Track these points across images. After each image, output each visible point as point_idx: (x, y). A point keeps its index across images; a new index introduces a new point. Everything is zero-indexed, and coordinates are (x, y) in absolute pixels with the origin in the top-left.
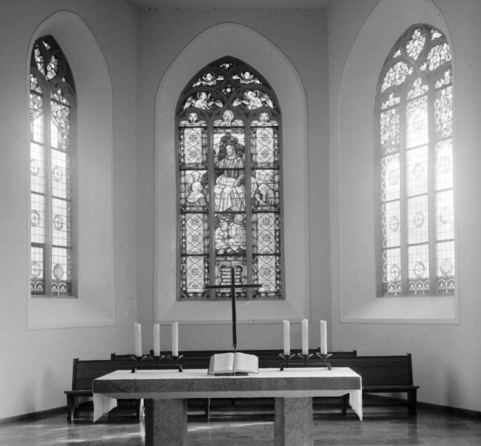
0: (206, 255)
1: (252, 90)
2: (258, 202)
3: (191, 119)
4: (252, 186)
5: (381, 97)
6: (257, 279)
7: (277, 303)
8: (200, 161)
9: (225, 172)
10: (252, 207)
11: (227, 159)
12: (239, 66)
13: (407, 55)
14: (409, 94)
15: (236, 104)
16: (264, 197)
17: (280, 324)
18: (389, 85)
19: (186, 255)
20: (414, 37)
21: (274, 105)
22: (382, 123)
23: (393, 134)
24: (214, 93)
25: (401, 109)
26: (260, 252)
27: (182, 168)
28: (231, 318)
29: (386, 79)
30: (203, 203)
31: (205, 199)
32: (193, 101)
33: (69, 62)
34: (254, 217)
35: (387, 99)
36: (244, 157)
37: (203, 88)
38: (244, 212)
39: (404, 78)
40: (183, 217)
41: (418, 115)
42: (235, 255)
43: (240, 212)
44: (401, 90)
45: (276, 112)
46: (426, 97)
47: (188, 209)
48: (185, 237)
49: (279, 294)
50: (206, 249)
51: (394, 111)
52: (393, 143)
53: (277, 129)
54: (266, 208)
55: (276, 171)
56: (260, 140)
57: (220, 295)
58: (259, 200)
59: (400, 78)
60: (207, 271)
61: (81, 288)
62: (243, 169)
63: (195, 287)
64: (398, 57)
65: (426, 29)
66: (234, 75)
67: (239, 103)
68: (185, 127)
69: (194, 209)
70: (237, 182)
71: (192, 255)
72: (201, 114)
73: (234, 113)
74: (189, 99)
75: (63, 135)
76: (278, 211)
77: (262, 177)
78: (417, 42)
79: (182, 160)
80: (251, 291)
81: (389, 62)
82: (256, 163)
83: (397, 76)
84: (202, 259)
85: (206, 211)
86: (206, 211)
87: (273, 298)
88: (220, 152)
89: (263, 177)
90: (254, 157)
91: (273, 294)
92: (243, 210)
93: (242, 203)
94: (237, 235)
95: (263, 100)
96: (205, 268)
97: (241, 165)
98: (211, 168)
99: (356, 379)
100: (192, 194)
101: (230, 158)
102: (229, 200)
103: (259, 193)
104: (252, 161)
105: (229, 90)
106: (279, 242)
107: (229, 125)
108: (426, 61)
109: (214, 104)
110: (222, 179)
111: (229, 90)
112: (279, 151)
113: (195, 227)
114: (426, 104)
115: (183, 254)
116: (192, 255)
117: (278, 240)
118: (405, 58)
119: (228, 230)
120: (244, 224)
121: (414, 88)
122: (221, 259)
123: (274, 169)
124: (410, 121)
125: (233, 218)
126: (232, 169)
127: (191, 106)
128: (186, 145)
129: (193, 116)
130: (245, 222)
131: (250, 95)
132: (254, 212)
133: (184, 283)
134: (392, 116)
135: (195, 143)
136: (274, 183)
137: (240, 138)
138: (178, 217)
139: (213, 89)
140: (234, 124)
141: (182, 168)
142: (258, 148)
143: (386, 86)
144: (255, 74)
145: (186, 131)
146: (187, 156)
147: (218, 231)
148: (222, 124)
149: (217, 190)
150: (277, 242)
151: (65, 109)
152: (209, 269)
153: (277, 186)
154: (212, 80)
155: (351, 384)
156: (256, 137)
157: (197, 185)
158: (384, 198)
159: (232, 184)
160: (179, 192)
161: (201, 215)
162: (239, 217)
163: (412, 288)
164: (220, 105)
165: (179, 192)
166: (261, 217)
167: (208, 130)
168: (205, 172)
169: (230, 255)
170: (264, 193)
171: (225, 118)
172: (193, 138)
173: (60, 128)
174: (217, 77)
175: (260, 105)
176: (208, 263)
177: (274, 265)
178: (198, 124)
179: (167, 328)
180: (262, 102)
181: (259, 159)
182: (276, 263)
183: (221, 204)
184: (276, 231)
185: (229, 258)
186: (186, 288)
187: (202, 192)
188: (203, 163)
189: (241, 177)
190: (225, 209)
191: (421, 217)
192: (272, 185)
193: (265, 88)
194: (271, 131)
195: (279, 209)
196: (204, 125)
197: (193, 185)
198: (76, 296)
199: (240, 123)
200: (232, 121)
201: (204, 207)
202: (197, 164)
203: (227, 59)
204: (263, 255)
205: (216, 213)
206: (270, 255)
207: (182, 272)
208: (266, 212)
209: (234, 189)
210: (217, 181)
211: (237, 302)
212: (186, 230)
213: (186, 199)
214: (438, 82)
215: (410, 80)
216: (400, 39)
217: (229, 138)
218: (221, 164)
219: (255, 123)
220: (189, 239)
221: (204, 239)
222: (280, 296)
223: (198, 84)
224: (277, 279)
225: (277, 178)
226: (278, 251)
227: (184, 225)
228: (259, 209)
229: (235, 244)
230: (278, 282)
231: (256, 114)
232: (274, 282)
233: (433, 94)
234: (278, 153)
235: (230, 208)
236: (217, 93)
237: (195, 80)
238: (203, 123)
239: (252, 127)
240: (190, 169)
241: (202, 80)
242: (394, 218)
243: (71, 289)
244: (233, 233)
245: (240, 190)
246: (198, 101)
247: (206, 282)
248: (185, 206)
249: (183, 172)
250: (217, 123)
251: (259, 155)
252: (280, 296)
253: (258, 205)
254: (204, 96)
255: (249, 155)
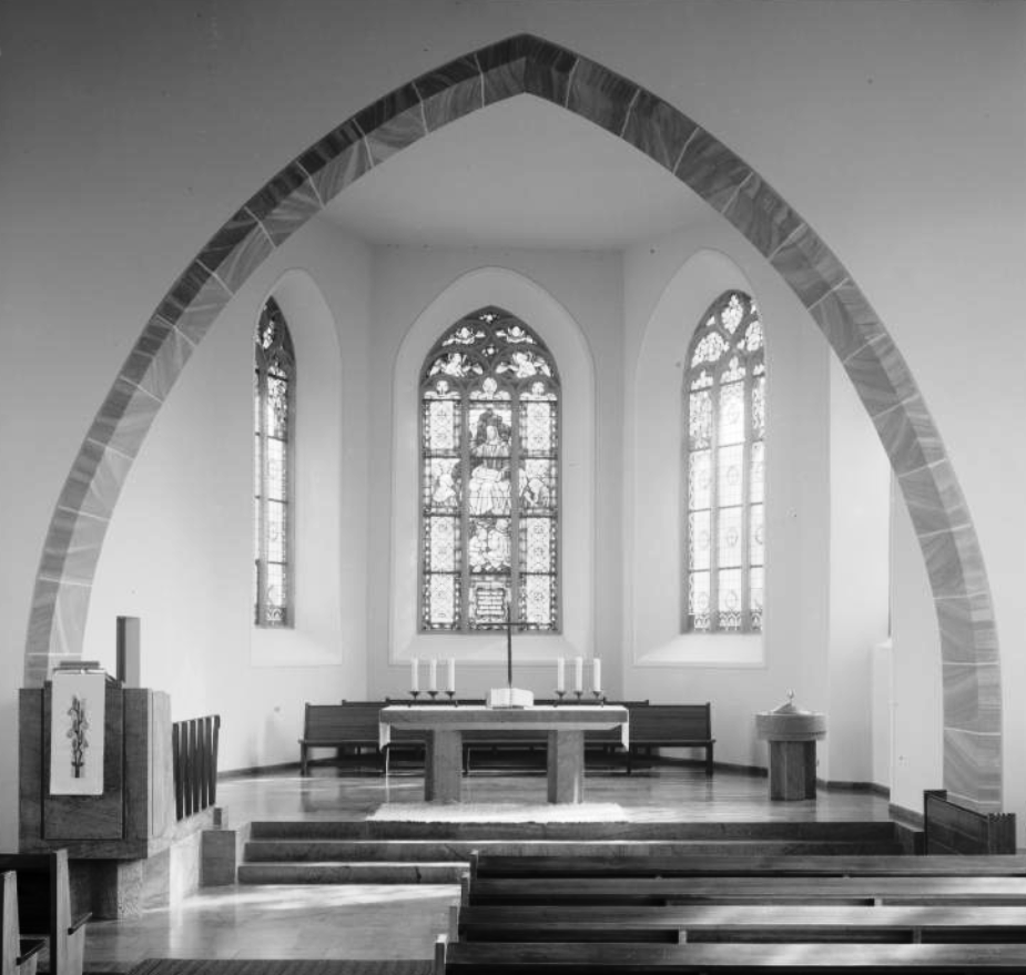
0: (458, 574)
1: (522, 351)
2: (529, 503)
3: (439, 389)
4: (521, 481)
5: (691, 374)
6: (525, 607)
7: (552, 639)
8: (451, 447)
9: (485, 462)
10: (520, 509)
11: (488, 444)
12: (505, 319)
13: (722, 325)
14: (724, 376)
15: (501, 369)
16: (536, 497)
17: (555, 666)
18: (700, 360)
19: (430, 573)
20: (730, 304)
21: (551, 372)
22: (692, 408)
23: (705, 425)
24: (472, 355)
25: (715, 391)
26: (529, 569)
27: (426, 455)
28: (507, 659)
29: (697, 351)
30: (454, 503)
31: (457, 497)
32: (443, 365)
33: (289, 325)
34: (523, 523)
35: (698, 377)
36: (510, 442)
37: (456, 348)
38: (509, 517)
39: (718, 354)
40: (427, 521)
41: (733, 402)
42: (495, 573)
43: (503, 517)
44: (715, 369)
45: (554, 384)
46: (742, 383)
47: (433, 510)
48: (428, 549)
49: (555, 628)
50: (457, 565)
51: (705, 394)
52: (704, 435)
53: (555, 405)
54: (539, 511)
55: (553, 462)
56: (533, 419)
57: (475, 627)
58: (529, 499)
59: (714, 353)
60: (457, 594)
61: (301, 611)
62: (509, 458)
63: (442, 615)
64: (711, 326)
65: (745, 299)
66: (499, 329)
67: (505, 369)
68: (431, 400)
69: (442, 510)
70: (500, 474)
71: (438, 573)
72: (454, 383)
73: (497, 382)
74: (438, 362)
75: (279, 418)
76: (555, 515)
77: (535, 470)
78: (734, 311)
79: (427, 445)
80: (513, 625)
81: (701, 331)
82: (526, 451)
83: (711, 350)
84: (451, 578)
85: (459, 513)
86: (459, 513)
87: (546, 632)
88: (479, 434)
89: (534, 473)
90: (524, 442)
91: (546, 627)
92: (508, 513)
93: (507, 503)
94: (499, 546)
95: (537, 365)
96: (456, 590)
97: (506, 453)
98: (466, 457)
99: (623, 713)
100: (440, 490)
101: (492, 443)
102: (490, 499)
103: (530, 491)
104: (521, 447)
105: (491, 351)
106: (555, 558)
107: (491, 398)
108: (744, 337)
109: (471, 371)
110: (480, 472)
111: (491, 351)
112: (557, 435)
113: (443, 535)
114: (742, 393)
115: (425, 571)
116: (438, 573)
117: (554, 554)
118: (719, 328)
119: (487, 540)
120: (509, 532)
121: (730, 370)
122: (476, 578)
123: (550, 459)
124: (725, 411)
125: (494, 524)
126: (493, 458)
127: (440, 372)
128: (432, 424)
129: (443, 385)
130: (510, 529)
131: (519, 358)
132: (522, 516)
133: (427, 610)
134: (703, 401)
135: (445, 421)
136: (550, 477)
137: (506, 416)
138: (420, 522)
139: (470, 350)
140: (498, 397)
141: (426, 455)
142: (529, 430)
143: (697, 360)
144: (528, 331)
145: (433, 405)
146: (433, 439)
147: (473, 541)
148: (482, 397)
149: (473, 485)
150: (552, 558)
151: (281, 385)
152: (461, 592)
153: (553, 481)
154: (469, 337)
155: (620, 717)
156: (526, 416)
157: (447, 480)
158: (692, 504)
159: (492, 478)
160: (422, 487)
161: (451, 519)
162: (502, 523)
163: (723, 623)
164: (479, 371)
165: (422, 487)
166: (531, 524)
167: (463, 405)
168: (457, 461)
169: (489, 574)
170: (536, 491)
171: (485, 389)
172: (442, 415)
173: (277, 409)
174: (475, 333)
175: (532, 372)
176: (460, 584)
177: (548, 588)
178: (448, 396)
179: (442, 668)
180: (536, 368)
181: (531, 445)
182: (551, 585)
183: (477, 506)
184: (551, 542)
185: (488, 578)
186: (430, 617)
187: (453, 487)
188: (455, 449)
189: (506, 468)
190: (483, 512)
191: (735, 535)
192: (547, 480)
193: (539, 350)
194: (547, 407)
195: (556, 513)
196: (457, 398)
197: (441, 478)
198: (292, 626)
199: (505, 395)
200: (495, 393)
201: (455, 508)
202: (447, 451)
203: (490, 310)
204: (534, 574)
205: (472, 516)
206: (542, 574)
207: (424, 595)
208: (538, 516)
209: (496, 485)
210: (473, 474)
211: (513, 638)
212: (430, 539)
213: (431, 497)
214: (756, 368)
215: (726, 357)
216: (713, 305)
217: (491, 416)
218: (480, 451)
219: (525, 396)
220: (434, 551)
221: (455, 551)
222: (555, 630)
223: (450, 341)
224: (551, 607)
225: (554, 471)
226: (553, 570)
227: (427, 533)
228: (530, 512)
229: (498, 558)
230: (553, 611)
231: (527, 384)
232: (547, 611)
233: (751, 381)
234: (557, 437)
235: (490, 511)
236: (476, 356)
237: (446, 336)
238: (455, 395)
239: (521, 402)
240: (437, 456)
241: (455, 336)
242: (704, 532)
243: (286, 618)
244: (493, 544)
245: (505, 485)
246: (449, 366)
247: (457, 610)
248: (430, 507)
249: (427, 461)
250: (475, 395)
251: (531, 440)
252: (555, 630)
253: (528, 508)
254: (457, 358)
255: (517, 440)
